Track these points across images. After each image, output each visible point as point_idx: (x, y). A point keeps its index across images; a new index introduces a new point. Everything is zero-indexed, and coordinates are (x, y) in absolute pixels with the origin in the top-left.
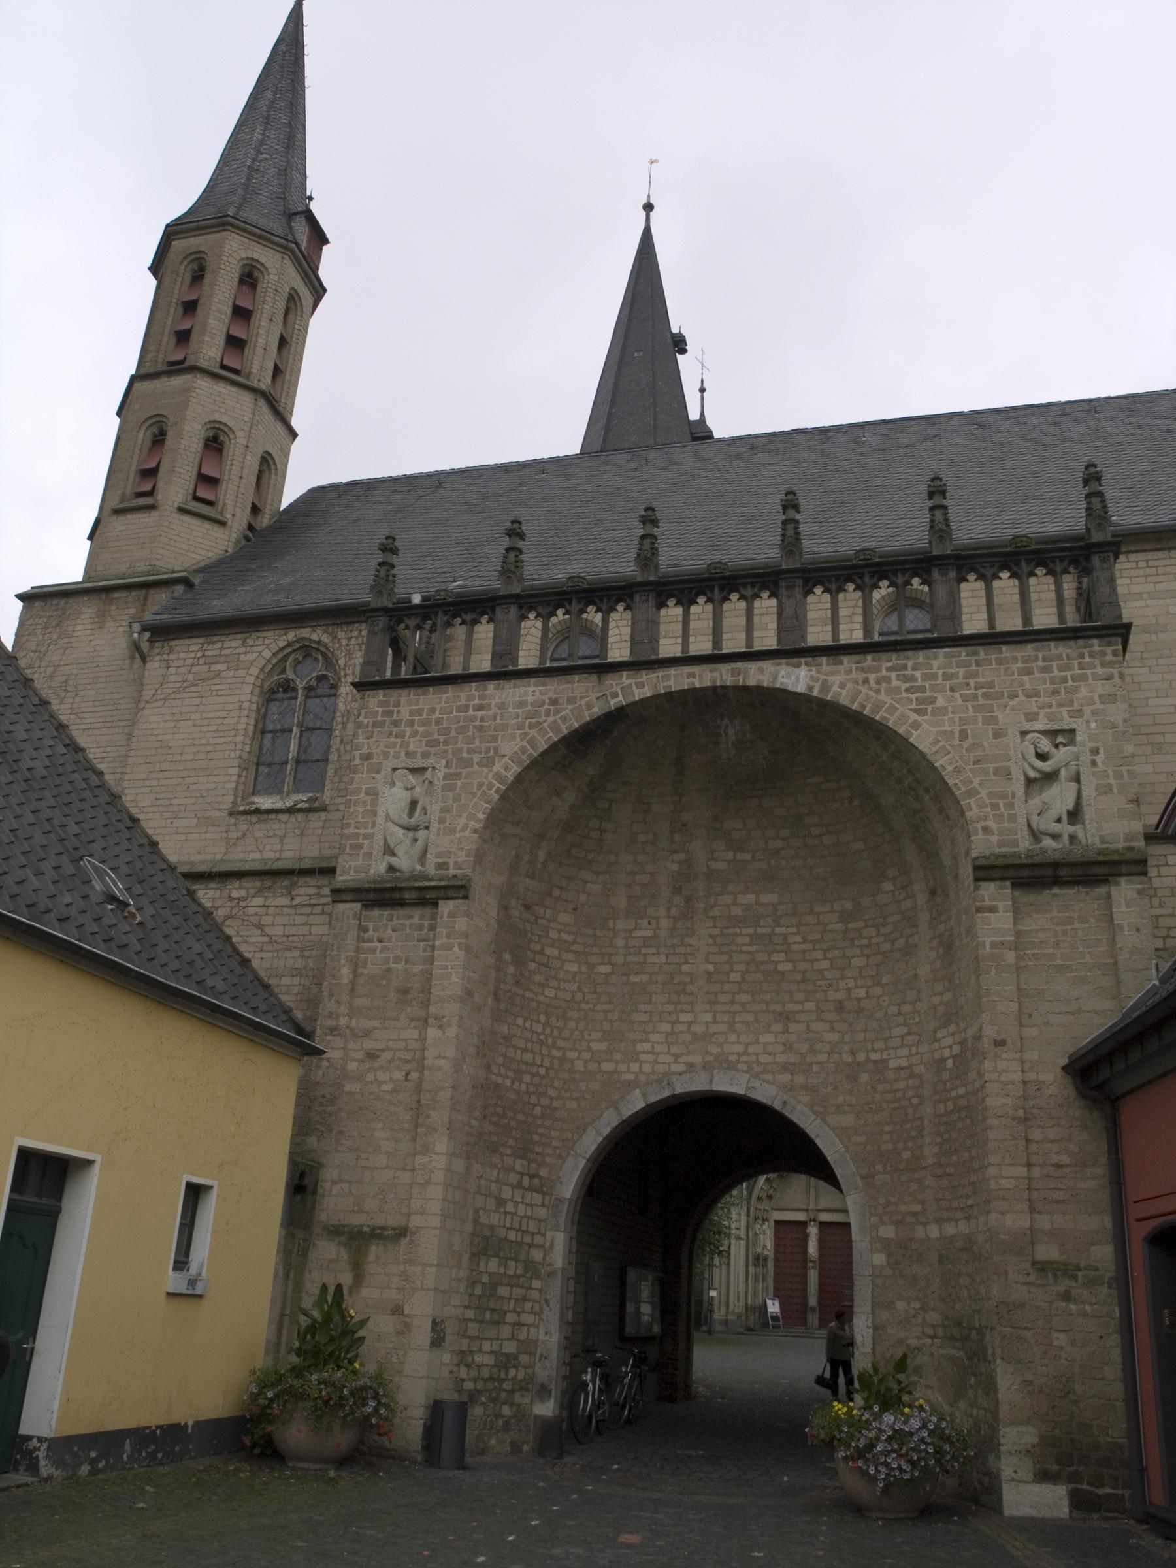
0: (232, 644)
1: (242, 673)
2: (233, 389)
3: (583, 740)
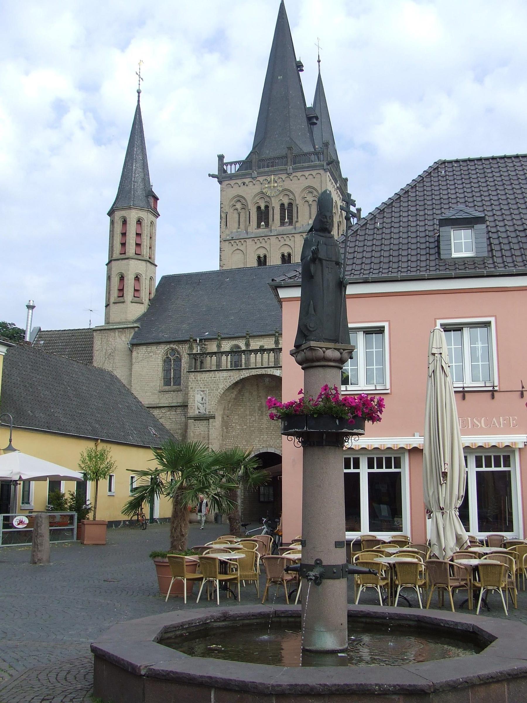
0: (154, 348)
1: (157, 356)
2: (140, 261)
3: (236, 384)
